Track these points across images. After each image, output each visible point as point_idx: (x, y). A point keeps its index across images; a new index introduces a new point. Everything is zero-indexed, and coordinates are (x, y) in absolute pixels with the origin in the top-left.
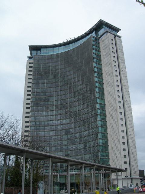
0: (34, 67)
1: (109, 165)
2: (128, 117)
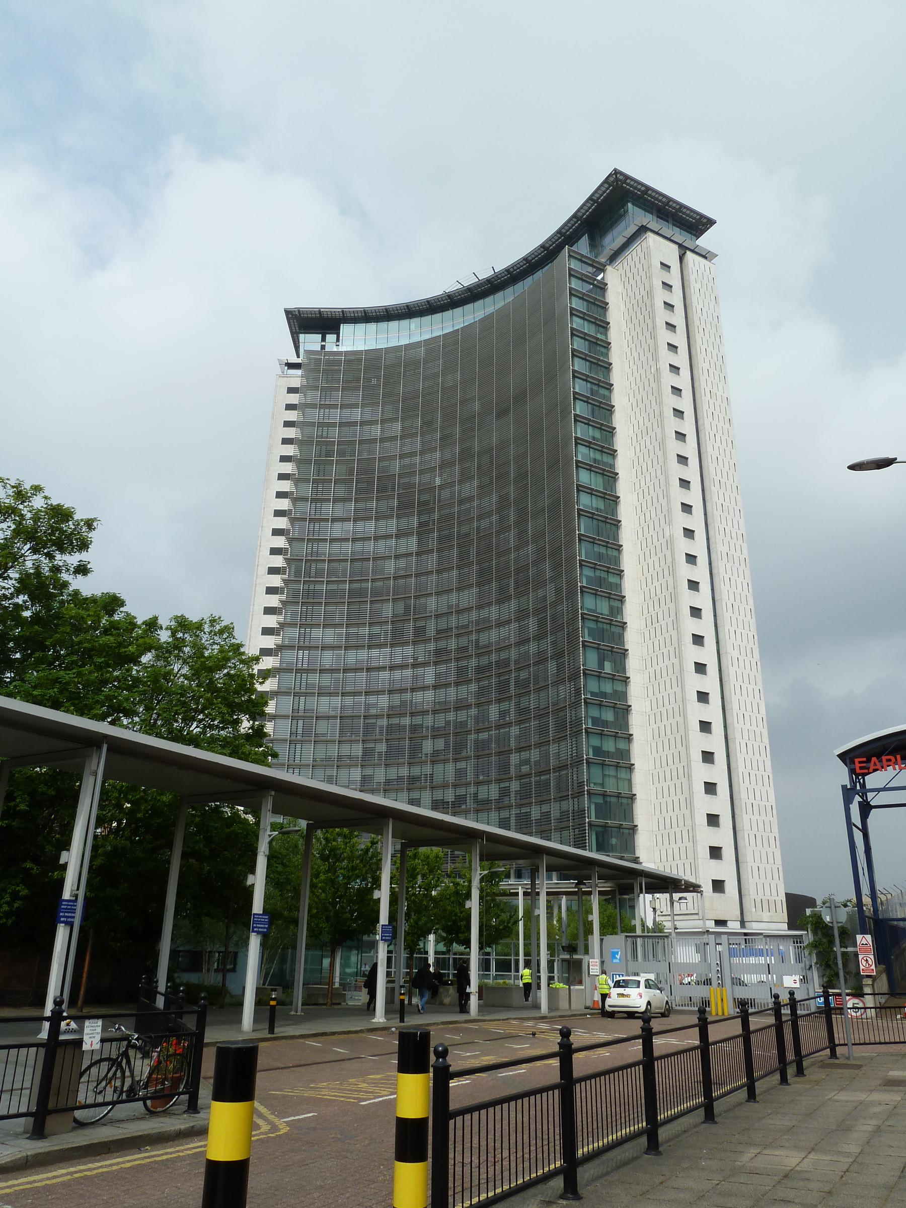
0: (300, 462)
1: (636, 860)
2: (701, 330)
